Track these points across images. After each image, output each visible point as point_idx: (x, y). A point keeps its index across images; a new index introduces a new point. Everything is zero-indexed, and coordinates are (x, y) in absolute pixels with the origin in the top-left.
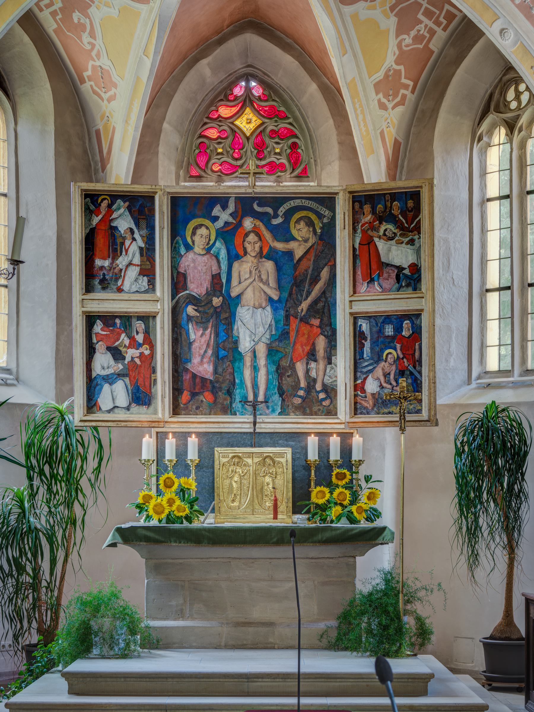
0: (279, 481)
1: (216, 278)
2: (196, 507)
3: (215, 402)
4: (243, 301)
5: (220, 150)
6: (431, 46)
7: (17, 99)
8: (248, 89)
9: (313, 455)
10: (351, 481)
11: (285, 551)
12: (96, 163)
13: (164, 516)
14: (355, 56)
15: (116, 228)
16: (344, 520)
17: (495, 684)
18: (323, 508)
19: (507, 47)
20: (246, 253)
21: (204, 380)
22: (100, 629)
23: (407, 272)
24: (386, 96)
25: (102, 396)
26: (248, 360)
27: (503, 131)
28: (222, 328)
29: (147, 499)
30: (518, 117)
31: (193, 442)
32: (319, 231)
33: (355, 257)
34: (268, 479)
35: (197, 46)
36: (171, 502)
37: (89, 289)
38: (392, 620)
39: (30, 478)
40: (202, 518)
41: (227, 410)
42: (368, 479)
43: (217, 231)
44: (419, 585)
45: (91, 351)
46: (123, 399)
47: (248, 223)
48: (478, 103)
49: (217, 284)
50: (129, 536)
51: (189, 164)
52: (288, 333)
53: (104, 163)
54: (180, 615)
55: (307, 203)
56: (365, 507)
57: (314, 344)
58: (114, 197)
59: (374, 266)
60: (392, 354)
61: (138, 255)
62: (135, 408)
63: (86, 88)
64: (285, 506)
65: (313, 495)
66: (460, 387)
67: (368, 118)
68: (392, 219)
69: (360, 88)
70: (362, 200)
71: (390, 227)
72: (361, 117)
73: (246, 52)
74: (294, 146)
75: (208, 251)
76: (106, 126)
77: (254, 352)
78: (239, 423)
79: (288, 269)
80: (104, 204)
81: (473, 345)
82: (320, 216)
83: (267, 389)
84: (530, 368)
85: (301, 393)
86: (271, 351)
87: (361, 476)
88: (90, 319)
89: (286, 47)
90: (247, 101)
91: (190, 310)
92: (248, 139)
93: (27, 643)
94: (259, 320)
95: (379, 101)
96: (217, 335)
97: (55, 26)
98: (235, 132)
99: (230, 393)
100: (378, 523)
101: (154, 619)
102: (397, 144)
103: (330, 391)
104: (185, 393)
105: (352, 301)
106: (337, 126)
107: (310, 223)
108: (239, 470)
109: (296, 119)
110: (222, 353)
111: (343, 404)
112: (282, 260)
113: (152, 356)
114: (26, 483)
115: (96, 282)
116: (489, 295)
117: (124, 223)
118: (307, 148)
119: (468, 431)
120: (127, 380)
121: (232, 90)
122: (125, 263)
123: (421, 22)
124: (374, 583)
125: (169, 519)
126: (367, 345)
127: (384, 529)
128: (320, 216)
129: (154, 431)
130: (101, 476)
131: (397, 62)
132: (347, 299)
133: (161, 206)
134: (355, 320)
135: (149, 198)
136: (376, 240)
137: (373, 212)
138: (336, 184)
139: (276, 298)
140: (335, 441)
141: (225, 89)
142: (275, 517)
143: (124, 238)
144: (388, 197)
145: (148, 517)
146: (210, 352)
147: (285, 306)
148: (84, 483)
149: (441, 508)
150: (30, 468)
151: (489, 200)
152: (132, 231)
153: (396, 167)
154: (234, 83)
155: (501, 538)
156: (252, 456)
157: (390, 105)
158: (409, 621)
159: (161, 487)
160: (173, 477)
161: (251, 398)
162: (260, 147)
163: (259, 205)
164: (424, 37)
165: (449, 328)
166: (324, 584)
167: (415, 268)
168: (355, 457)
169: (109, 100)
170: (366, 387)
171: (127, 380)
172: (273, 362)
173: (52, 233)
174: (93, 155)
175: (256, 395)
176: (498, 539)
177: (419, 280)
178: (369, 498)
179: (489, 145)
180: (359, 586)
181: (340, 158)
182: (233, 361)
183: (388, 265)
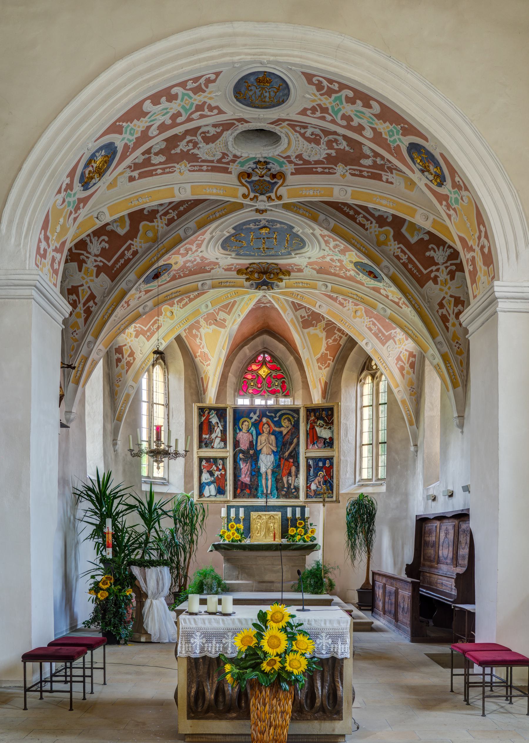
0: (276, 526)
1: (251, 443)
2: (243, 536)
4: (262, 452)
5: (252, 384)
6: (340, 343)
7: (169, 364)
8: (264, 358)
9: (289, 515)
10: (305, 525)
11: (278, 553)
12: (201, 391)
13: (230, 539)
14: (308, 349)
15: (211, 422)
16: (301, 541)
17: (362, 608)
18: (293, 536)
19: (368, 350)
20: (263, 432)
21: (246, 484)
22: (207, 583)
23: (328, 440)
24: (322, 364)
25: (205, 491)
26: (264, 476)
27: (370, 378)
28: (254, 463)
29: (224, 533)
30: (376, 373)
31: (242, 510)
32: (293, 423)
33: (307, 434)
34: (272, 525)
35: (243, 341)
36: (233, 534)
37: (200, 447)
38: (319, 580)
39: (176, 524)
40: (245, 540)
41: (255, 496)
42: (311, 525)
43: (252, 423)
44: (330, 566)
45: (201, 472)
46: (213, 492)
47: (264, 420)
48: (360, 365)
49: (252, 446)
50: (217, 547)
51: (239, 389)
52: (280, 465)
53: (205, 391)
54: (237, 579)
55: (288, 412)
56: (310, 536)
57: (290, 469)
58: (210, 409)
59: (315, 438)
60: (322, 473)
61: (220, 433)
62: (218, 496)
63: (197, 360)
64: (278, 535)
65: (289, 531)
66: (351, 485)
67: (314, 374)
68: (322, 419)
69: (311, 362)
70: (310, 411)
71: (322, 422)
72: (311, 373)
73: (263, 343)
74: (284, 382)
75: (248, 431)
76: (206, 376)
77: (266, 473)
78: (260, 502)
79: (280, 439)
80: (207, 412)
81: (357, 468)
82: (293, 417)
83: (271, 488)
84: (380, 478)
85: (285, 489)
86: (273, 472)
87: (309, 523)
88: (201, 459)
89: (280, 341)
90: (264, 363)
91: (241, 455)
92: (264, 379)
93: (174, 591)
94: (268, 459)
95: (319, 366)
96: (252, 466)
97: (185, 335)
98: (259, 376)
99: (256, 489)
100: (315, 542)
101: (227, 580)
102: (326, 383)
103: (297, 489)
104: (239, 489)
105: (305, 452)
106: (302, 375)
107: (289, 420)
108: (260, 521)
109: (284, 371)
110: (254, 473)
111: (302, 494)
112: (278, 435)
113: (225, 474)
114: (174, 526)
115: (203, 444)
116: (363, 447)
117: (214, 420)
118: (289, 383)
119: (354, 504)
120: (215, 484)
122: (215, 436)
123: (336, 334)
124: (313, 566)
125: (232, 541)
126: (312, 470)
127: (317, 544)
128: (293, 417)
129: (226, 505)
130: (204, 523)
131: (326, 350)
132: (304, 451)
133: (229, 413)
134: (307, 460)
135: (224, 410)
136: (316, 427)
137: (315, 416)
138: (301, 404)
139: (275, 451)
140: (298, 510)
141: (255, 357)
142: (274, 540)
143: (214, 426)
144: (321, 410)
145: (224, 540)
146: (249, 473)
147: (278, 453)
148: (198, 526)
149: (341, 537)
150: (175, 520)
151: (364, 407)
152: (218, 423)
153: (326, 393)
154: (258, 355)
155: (364, 548)
156: (265, 515)
157: (323, 368)
159: (229, 528)
160: (234, 524)
161: (265, 491)
162: (269, 383)
164: (337, 339)
165: (347, 461)
166: (293, 566)
167: (331, 439)
168: (306, 516)
169: (207, 366)
170: (460, 316)
171: (215, 484)
172: (274, 477)
173: (183, 421)
175: (267, 491)
176: (363, 548)
177: (333, 444)
178: (311, 532)
179: (364, 383)
180: (307, 567)
181: (303, 388)
182: (258, 477)
183: (320, 437)
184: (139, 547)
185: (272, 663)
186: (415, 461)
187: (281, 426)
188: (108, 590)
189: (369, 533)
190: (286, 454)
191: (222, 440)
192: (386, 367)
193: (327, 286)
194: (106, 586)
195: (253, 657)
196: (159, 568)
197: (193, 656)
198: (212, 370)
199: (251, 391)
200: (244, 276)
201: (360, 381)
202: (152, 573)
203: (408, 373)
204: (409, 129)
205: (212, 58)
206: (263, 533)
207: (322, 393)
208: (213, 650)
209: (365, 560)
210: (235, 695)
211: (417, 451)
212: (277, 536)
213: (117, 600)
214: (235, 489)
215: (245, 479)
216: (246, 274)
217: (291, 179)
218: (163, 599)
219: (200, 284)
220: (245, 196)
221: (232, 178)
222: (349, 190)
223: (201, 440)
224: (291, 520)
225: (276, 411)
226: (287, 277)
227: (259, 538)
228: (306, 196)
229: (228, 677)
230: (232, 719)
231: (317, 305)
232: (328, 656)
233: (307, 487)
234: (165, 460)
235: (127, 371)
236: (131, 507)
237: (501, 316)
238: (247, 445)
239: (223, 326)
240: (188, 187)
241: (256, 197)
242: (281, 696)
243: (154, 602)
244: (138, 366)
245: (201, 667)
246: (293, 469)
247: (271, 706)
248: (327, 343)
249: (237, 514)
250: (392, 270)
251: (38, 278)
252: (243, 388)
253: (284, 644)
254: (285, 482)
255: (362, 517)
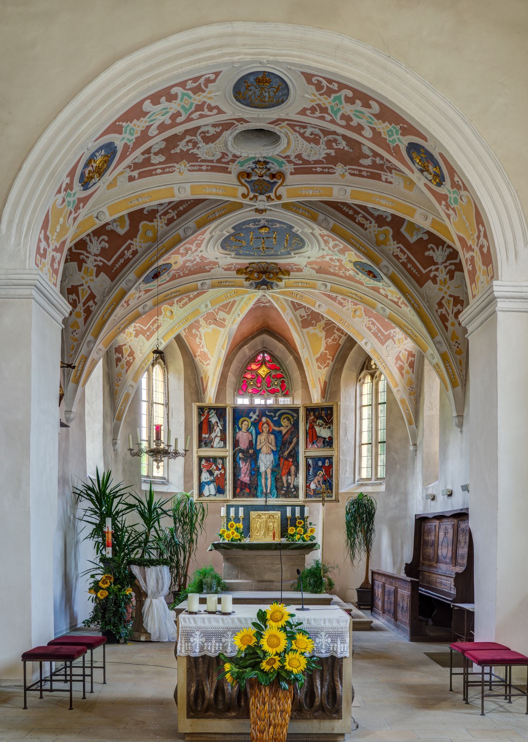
0: (276, 525)
1: (251, 442)
2: (243, 535)
3: (250, 492)
4: (262, 451)
5: (252, 384)
6: (340, 342)
7: (168, 364)
8: (264, 357)
9: (289, 514)
10: (304, 525)
11: (277, 552)
12: (201, 390)
13: (230, 539)
14: (308, 348)
15: (211, 421)
16: (301, 540)
17: (361, 607)
18: (293, 536)
19: (368, 349)
20: (263, 432)
21: (246, 484)
22: (207, 582)
23: (327, 440)
24: (321, 363)
25: (205, 490)
26: (263, 475)
27: (369, 377)
28: (253, 462)
29: (224, 532)
30: (375, 372)
31: (241, 510)
32: (292, 423)
33: (307, 433)
34: (271, 524)
35: (243, 340)
36: (233, 533)
37: (200, 446)
38: (318, 579)
39: (175, 523)
40: (245, 540)
41: (255, 496)
42: (310, 524)
43: (252, 423)
44: (329, 566)
45: (200, 472)
46: (213, 492)
47: (264, 419)
48: (359, 365)
49: (252, 445)
50: (217, 546)
51: (239, 389)
52: (279, 464)
53: (204, 391)
54: (237, 578)
55: (287, 411)
56: (309, 535)
57: (290, 469)
58: (210, 408)
59: (314, 437)
60: (321, 473)
61: (219, 432)
62: (218, 495)
63: (197, 359)
64: (278, 534)
65: (289, 530)
66: (350, 485)
67: (313, 373)
68: (321, 418)
69: (310, 361)
70: (309, 410)
71: (321, 421)
72: (310, 373)
73: (263, 342)
74: (283, 382)
75: (248, 431)
76: (205, 375)
77: (266, 472)
78: (260, 501)
79: (280, 438)
80: (206, 412)
81: (356, 467)
82: (293, 417)
83: (271, 487)
84: (379, 477)
85: (285, 489)
86: (273, 472)
87: (308, 523)
88: (200, 459)
89: (280, 341)
90: (263, 363)
91: (240, 455)
92: (264, 378)
93: (174, 590)
94: (268, 459)
95: (318, 366)
96: (251, 465)
97: (185, 334)
98: (258, 376)
99: (256, 489)
100: (314, 542)
101: (227, 579)
102: (325, 383)
103: (296, 488)
104: (238, 489)
105: (305, 451)
106: (301, 375)
107: (289, 420)
108: (260, 520)
109: (284, 370)
110: (253, 473)
111: (301, 493)
112: (277, 434)
113: (225, 473)
114: (174, 525)
115: (203, 444)
116: (363, 446)
117: (214, 419)
118: (288, 383)
119: (353, 503)
120: (215, 483)
121: (257, 358)
122: (214, 436)
123: (335, 333)
124: (312, 565)
125: (232, 540)
126: (311, 469)
127: (316, 544)
128: (293, 417)
129: (225, 504)
130: (204, 522)
131: (325, 350)
132: (304, 451)
133: (229, 412)
134: (307, 459)
136: (315, 426)
137: (314, 415)
138: (300, 403)
139: (275, 450)
140: (298, 509)
141: (254, 357)
142: (274, 539)
143: (214, 426)
144: (320, 409)
145: (224, 539)
146: (248, 472)
147: (278, 453)
148: (197, 525)
149: (340, 536)
150: (175, 519)
151: (363, 406)
152: (217, 423)
154: (258, 355)
155: (364, 548)
156: (265, 514)
157: (322, 367)
158: (325, 580)
159: (229, 527)
160: (234, 523)
161: (264, 491)
162: (269, 382)
163: (268, 412)
164: (336, 339)
165: (346, 460)
166: (292, 565)
167: (331, 438)
168: (306, 515)
169: (207, 365)
171: (215, 483)
172: (274, 476)
174: (200, 387)
175: (266, 490)
176: (363, 547)
177: (332, 443)
178: (311, 532)
179: (363, 383)
180: (306, 566)
181: (302, 388)
182: (257, 476)
183: (320, 437)
184: (139, 547)
185: (271, 662)
186: (414, 460)
187: (280, 425)
188: (108, 589)
189: (368, 532)
190: (285, 453)
191: (221, 440)
192: (386, 367)
193: (326, 286)
194: (106, 586)
195: (253, 656)
196: (158, 567)
197: (192, 655)
198: (212, 369)
199: (250, 391)
200: (244, 276)
201: (359, 380)
202: (152, 572)
203: (407, 372)
204: (408, 129)
205: (212, 58)
206: (262, 533)
207: (322, 393)
208: (213, 649)
209: (364, 559)
210: (235, 694)
211: (416, 451)
212: (276, 535)
213: (116, 599)
214: (235, 488)
215: (245, 478)
216: (245, 273)
217: (290, 179)
218: (162, 598)
219: (199, 283)
220: (244, 196)
221: (232, 178)
222: (349, 189)
223: (200, 440)
224: (291, 519)
225: (276, 410)
226: (287, 277)
227: (259, 537)
228: (305, 196)
229: (228, 676)
230: (232, 718)
231: (317, 305)
232: (328, 655)
233: (307, 487)
234: (165, 459)
235: (127, 371)
236: (131, 506)
237: (500, 316)
238: (247, 444)
239: (223, 326)
240: (188, 186)
241: (255, 197)
242: (281, 695)
243: (154, 601)
244: (138, 366)
245: (201, 666)
246: (293, 468)
247: (271, 705)
248: (326, 343)
249: (237, 513)
250: (392, 269)
251: (38, 277)
252: (242, 388)
253: (283, 643)
254: (285, 481)
255: (361, 517)
